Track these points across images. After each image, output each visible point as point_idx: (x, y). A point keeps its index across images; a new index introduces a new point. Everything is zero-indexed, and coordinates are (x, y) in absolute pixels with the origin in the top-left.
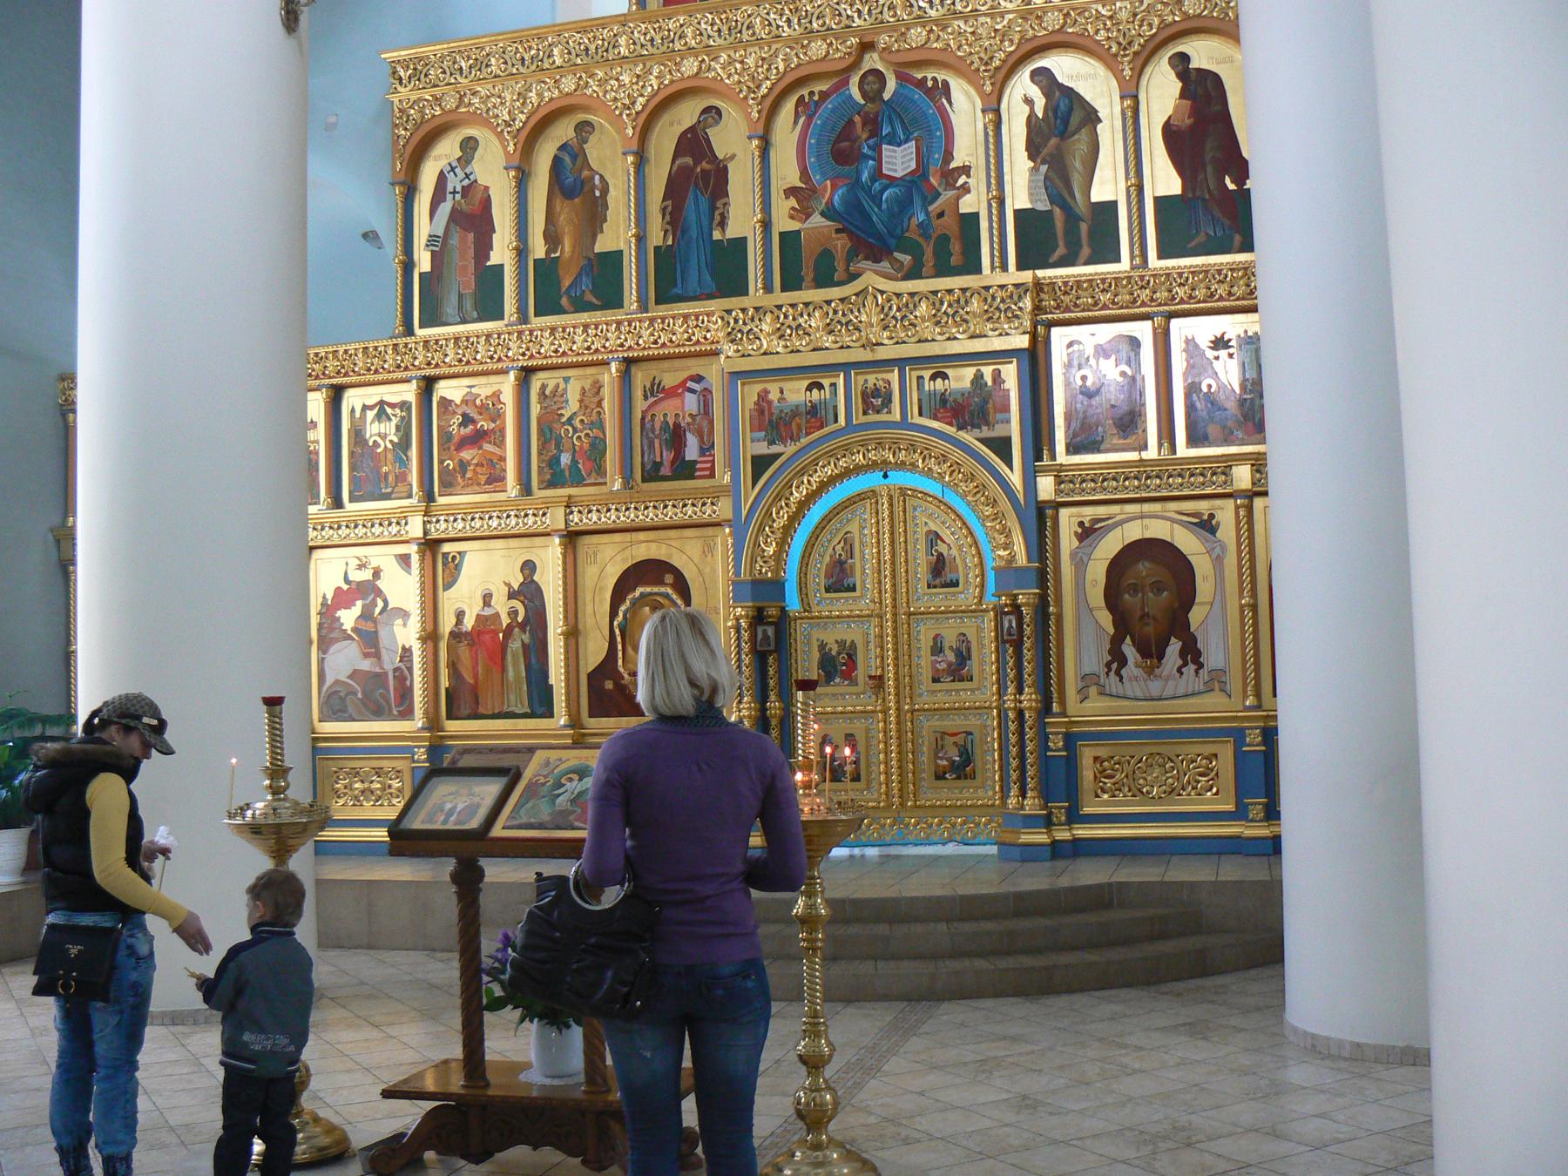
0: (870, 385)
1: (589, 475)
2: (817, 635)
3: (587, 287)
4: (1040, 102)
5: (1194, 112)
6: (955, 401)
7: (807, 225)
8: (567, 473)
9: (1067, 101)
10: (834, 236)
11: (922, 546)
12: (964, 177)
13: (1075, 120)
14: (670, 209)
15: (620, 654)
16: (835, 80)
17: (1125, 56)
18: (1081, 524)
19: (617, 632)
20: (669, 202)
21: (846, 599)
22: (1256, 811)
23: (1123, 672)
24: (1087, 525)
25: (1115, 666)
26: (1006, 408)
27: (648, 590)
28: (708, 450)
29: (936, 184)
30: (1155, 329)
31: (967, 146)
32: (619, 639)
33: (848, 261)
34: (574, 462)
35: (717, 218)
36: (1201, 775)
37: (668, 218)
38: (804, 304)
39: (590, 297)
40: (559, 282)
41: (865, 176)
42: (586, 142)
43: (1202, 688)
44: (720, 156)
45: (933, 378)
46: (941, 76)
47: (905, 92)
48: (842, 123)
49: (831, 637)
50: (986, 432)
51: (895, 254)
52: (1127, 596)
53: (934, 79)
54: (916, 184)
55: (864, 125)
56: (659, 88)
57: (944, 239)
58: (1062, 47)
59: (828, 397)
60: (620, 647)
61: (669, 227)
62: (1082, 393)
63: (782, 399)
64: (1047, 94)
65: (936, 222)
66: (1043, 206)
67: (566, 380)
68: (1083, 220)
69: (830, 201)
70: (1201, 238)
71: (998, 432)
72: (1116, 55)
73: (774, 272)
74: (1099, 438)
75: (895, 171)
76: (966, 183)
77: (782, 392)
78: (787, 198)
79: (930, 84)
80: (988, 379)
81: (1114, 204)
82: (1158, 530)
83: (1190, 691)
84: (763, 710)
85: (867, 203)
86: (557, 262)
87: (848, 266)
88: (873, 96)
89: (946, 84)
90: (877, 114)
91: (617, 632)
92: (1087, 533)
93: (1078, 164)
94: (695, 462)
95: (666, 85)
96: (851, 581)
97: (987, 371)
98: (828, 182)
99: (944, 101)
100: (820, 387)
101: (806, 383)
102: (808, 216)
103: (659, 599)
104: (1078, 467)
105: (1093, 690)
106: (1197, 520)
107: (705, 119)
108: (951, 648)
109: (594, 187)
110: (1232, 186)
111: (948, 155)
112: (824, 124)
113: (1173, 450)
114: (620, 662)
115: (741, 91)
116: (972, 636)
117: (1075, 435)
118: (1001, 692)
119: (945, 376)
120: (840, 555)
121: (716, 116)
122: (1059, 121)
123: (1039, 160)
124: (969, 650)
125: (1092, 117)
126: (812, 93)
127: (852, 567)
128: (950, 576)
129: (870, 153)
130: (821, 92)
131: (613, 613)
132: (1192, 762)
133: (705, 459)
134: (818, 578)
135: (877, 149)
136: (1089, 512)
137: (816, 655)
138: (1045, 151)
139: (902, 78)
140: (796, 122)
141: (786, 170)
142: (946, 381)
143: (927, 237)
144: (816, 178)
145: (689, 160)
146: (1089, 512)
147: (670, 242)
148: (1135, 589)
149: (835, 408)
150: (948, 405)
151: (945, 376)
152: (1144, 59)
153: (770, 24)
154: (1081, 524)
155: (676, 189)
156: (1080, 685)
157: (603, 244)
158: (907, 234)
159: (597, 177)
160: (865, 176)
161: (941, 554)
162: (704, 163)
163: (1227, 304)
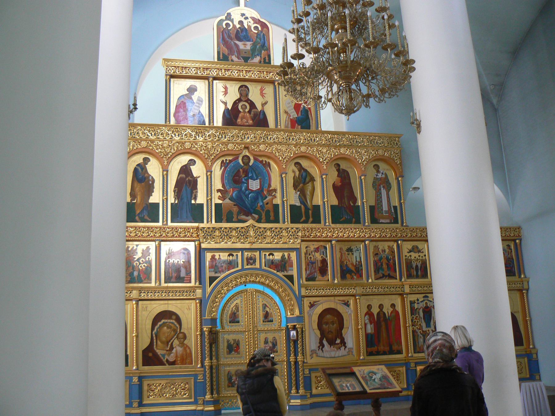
0: (249, 256)
1: (145, 279)
2: (226, 336)
3: (146, 214)
4: (297, 173)
5: (341, 181)
6: (276, 263)
7: (224, 202)
8: (136, 278)
9: (305, 173)
10: (233, 206)
11: (261, 308)
12: (274, 192)
13: (307, 180)
14: (177, 191)
15: (155, 344)
16: (234, 157)
17: (209, 159)
18: (310, 303)
19: (154, 335)
20: (177, 189)
21: (236, 325)
22: (135, 404)
23: (323, 349)
24: (312, 303)
25: (321, 347)
26: (292, 266)
27: (166, 321)
28: (189, 273)
29: (266, 194)
30: (195, 245)
31: (275, 183)
32: (155, 338)
33: (238, 215)
34: (139, 275)
35: (193, 196)
36: (183, 389)
37: (176, 194)
38: (291, 228)
39: (146, 217)
40: (135, 211)
41: (243, 189)
42: (147, 164)
43: (346, 354)
44: (195, 176)
45: (269, 255)
46: (268, 160)
47: (257, 164)
48: (236, 171)
49: (231, 337)
50: (286, 273)
51: (253, 214)
52: (324, 325)
53: (226, 160)
54: (259, 193)
55: (243, 172)
56: (132, 150)
57: (268, 212)
58: (194, 155)
59: (235, 258)
60: (155, 341)
61: (176, 197)
62: (310, 263)
63: (219, 258)
64: (300, 171)
65: (266, 206)
66: (298, 204)
67: (137, 245)
68: (310, 210)
69: (232, 195)
70: (344, 218)
71: (290, 273)
72: (207, 158)
73: (214, 216)
74: (315, 276)
75: (253, 188)
76: (275, 194)
77: (220, 256)
78: (218, 192)
79: (264, 162)
80: (286, 256)
81: (158, 204)
82: (332, 306)
83: (343, 354)
84: (296, 359)
85: (244, 197)
86: (135, 204)
87: (238, 217)
88: (246, 163)
89: (269, 163)
90: (247, 169)
91: (154, 335)
92: (312, 306)
93: (308, 193)
94: (184, 278)
95: (179, 150)
96: (238, 319)
97: (286, 254)
98: (231, 189)
99: (269, 168)
100: (233, 255)
101: (228, 254)
102: (224, 199)
103: (170, 324)
104: (167, 287)
105: (314, 355)
106: (343, 303)
107: (190, 163)
108: (271, 342)
109: (149, 180)
110: (352, 204)
111: (270, 185)
112: (230, 170)
113: (160, 284)
114: (155, 346)
115: (161, 155)
116: (277, 338)
117: (308, 275)
118: (288, 355)
119: (273, 255)
120: (234, 311)
121: (194, 162)
122: (303, 179)
123: (297, 190)
124: (276, 343)
125: (312, 179)
126: (226, 160)
127: (238, 315)
128: (270, 319)
129: (245, 181)
130: (229, 160)
131: (153, 329)
132: (180, 385)
133: (188, 276)
134: (227, 318)
135: (247, 180)
136: (312, 300)
137: (226, 344)
138: (299, 188)
139: (255, 159)
140: (221, 168)
141: (218, 184)
142: (273, 256)
143: (263, 210)
144: (227, 187)
145: (184, 176)
146: (312, 300)
147: (177, 202)
148: (327, 323)
149: (238, 263)
150: (274, 264)
151: (273, 255)
152: (214, 161)
153: (145, 134)
154: (310, 303)
155: (179, 184)
156: (311, 353)
157: (152, 200)
158: (256, 209)
159: (151, 177)
160: (243, 189)
161: (267, 312)
162: (189, 177)
163: (415, 238)
